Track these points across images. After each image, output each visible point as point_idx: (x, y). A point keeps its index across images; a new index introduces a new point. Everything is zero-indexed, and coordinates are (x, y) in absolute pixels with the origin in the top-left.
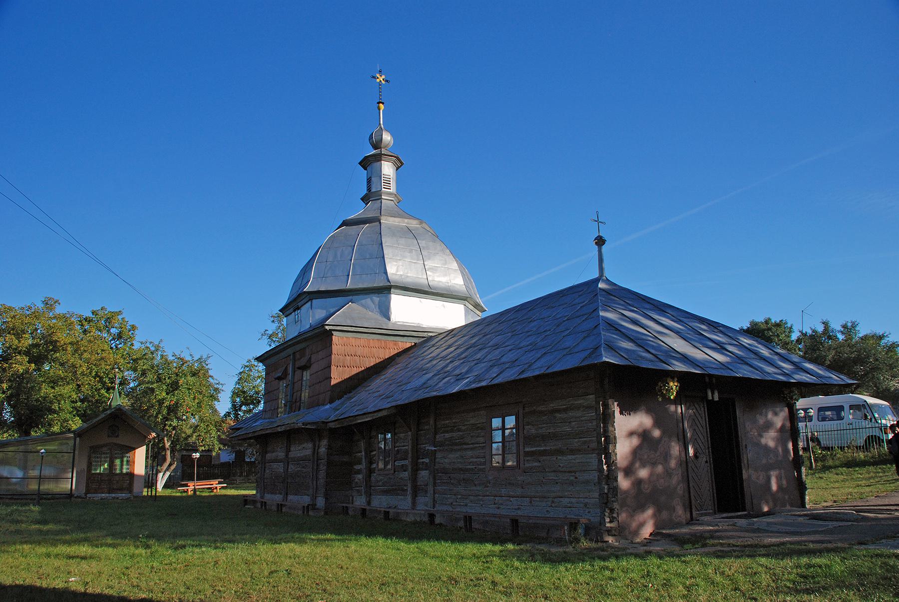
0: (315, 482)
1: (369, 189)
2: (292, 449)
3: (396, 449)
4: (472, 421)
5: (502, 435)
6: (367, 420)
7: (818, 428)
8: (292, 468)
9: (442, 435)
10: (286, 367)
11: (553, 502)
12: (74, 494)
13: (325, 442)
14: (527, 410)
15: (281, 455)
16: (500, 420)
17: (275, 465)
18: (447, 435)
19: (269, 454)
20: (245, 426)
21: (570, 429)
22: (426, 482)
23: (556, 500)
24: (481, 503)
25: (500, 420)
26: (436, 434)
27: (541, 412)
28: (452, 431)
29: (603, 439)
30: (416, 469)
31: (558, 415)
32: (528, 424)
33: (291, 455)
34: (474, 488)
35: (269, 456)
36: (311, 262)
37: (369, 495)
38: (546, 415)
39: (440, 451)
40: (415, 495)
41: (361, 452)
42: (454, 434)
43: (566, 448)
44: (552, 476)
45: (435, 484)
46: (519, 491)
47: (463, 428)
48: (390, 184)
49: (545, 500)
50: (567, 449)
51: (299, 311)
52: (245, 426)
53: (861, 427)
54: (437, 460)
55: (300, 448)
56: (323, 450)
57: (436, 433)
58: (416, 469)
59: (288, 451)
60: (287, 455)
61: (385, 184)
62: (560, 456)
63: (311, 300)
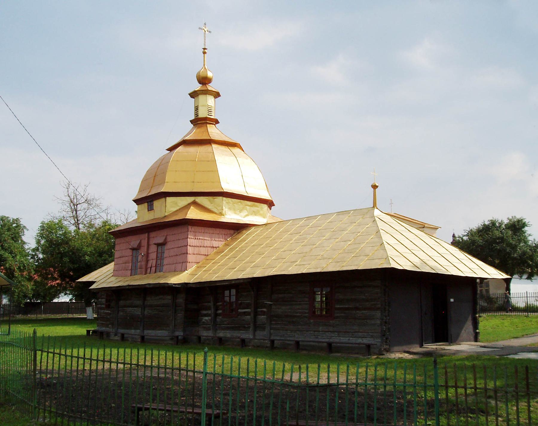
7: (520, 295)
18: (280, 296)
19: (122, 302)
24: (305, 335)
29: (39, 301)
30: (256, 314)
36: (316, 217)
40: (255, 330)
41: (209, 302)
46: (331, 329)
47: (293, 292)
48: (208, 111)
53: (522, 296)
58: (256, 314)
60: (144, 304)
61: (209, 112)
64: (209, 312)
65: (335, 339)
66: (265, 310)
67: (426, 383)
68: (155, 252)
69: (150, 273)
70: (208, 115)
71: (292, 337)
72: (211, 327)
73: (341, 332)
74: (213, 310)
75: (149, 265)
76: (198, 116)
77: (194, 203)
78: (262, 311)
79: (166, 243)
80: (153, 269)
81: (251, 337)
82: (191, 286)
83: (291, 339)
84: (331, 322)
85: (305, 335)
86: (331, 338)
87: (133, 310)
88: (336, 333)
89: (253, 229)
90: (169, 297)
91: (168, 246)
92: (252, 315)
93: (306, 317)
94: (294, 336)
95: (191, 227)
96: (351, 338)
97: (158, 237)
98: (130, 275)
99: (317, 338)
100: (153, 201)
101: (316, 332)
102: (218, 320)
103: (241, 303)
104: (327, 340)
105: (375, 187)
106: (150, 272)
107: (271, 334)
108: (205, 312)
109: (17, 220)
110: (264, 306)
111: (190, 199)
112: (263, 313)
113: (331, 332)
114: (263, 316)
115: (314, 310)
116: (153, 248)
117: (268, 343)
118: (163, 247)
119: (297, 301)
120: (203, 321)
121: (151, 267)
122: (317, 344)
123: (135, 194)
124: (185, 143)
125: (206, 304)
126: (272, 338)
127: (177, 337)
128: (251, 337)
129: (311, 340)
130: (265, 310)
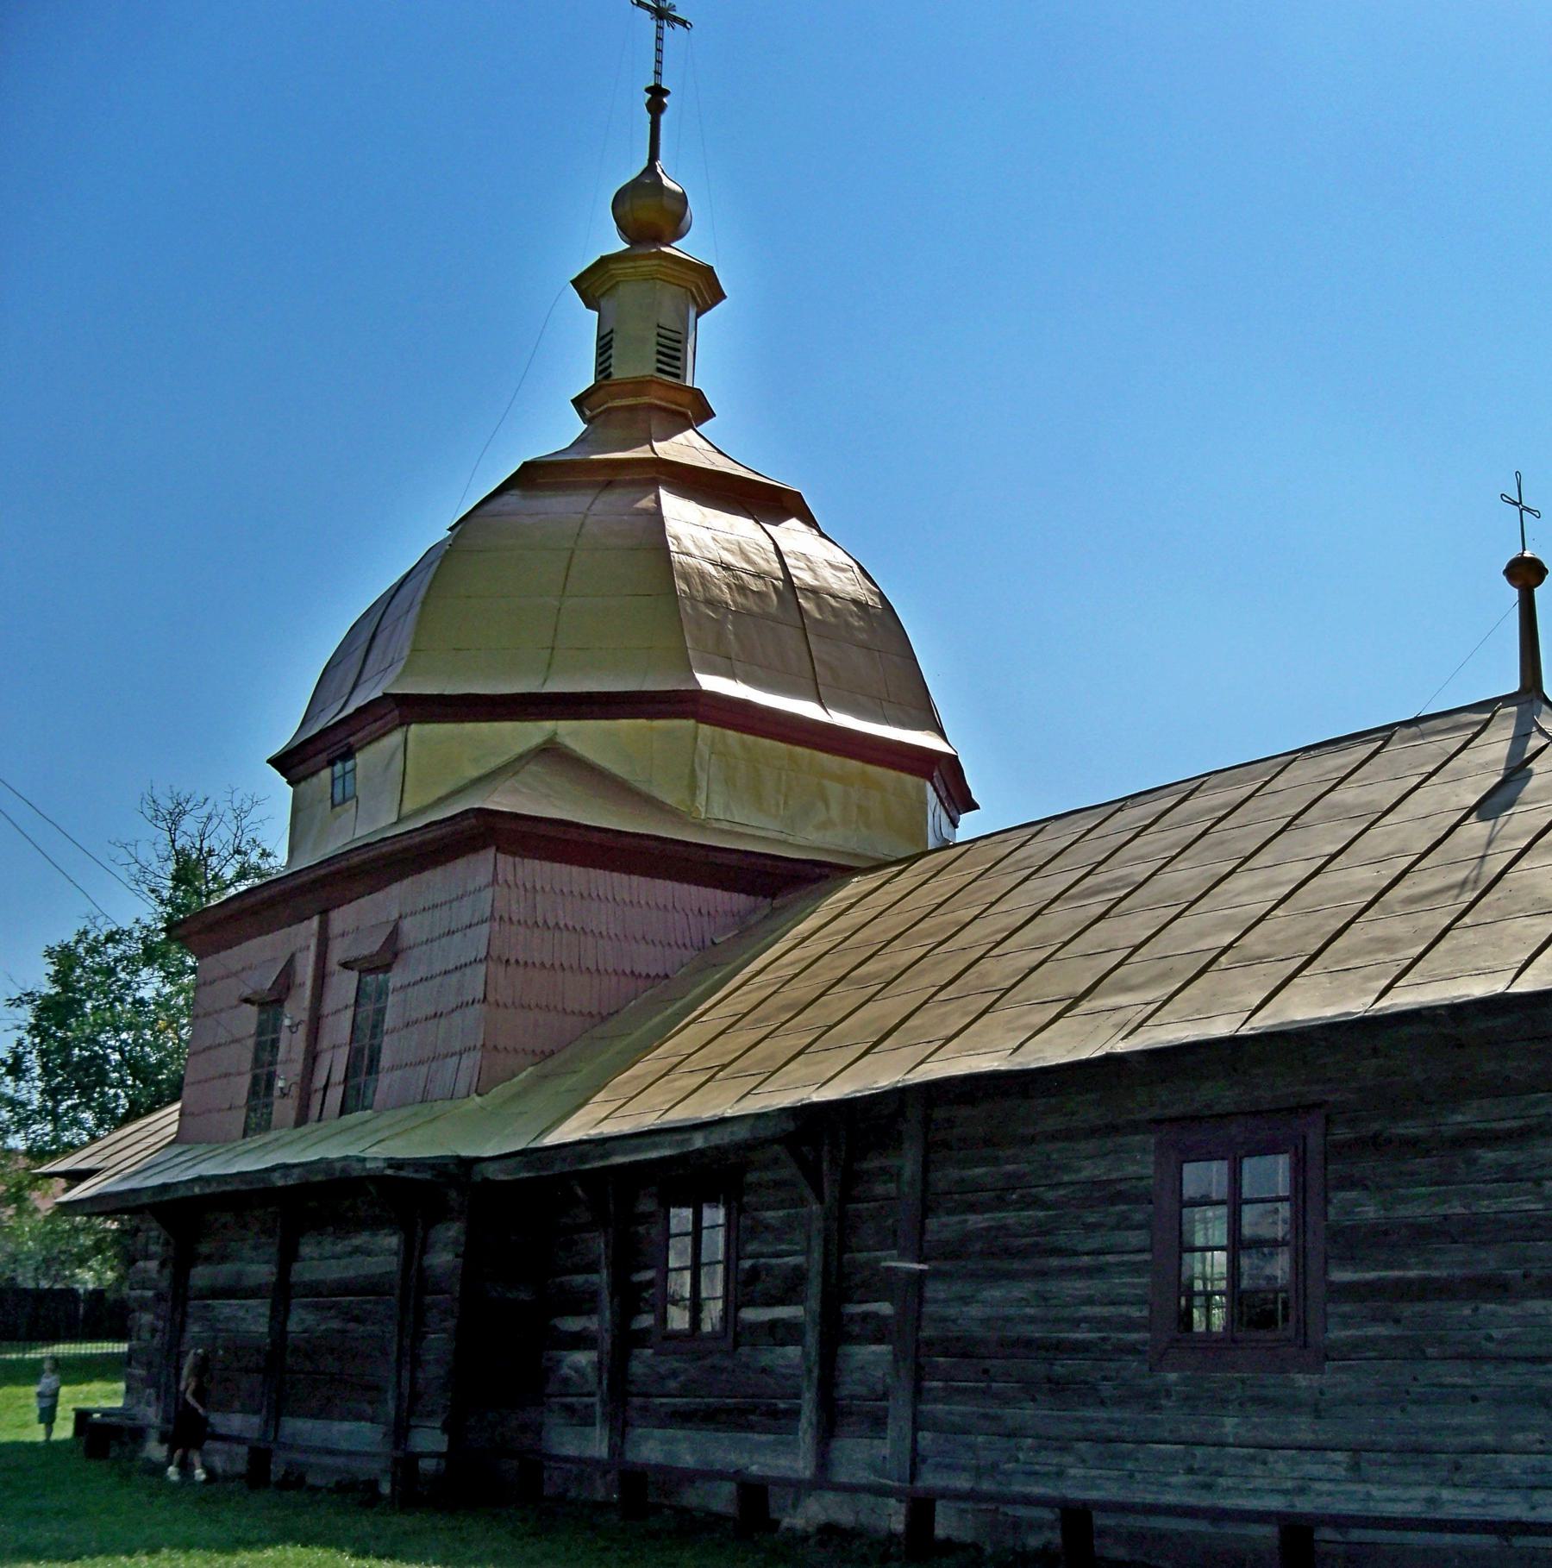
0: (406, 1374)
1: (603, 370)
2: (306, 1250)
3: (747, 1264)
4: (1090, 1171)
5: (700, 1249)
6: (654, 1155)
8: (300, 1320)
9: (955, 1219)
10: (291, 960)
11: (1457, 1467)
12: (632, 1382)
13: (452, 1231)
14: (1342, 1133)
15: (262, 1271)
16: (688, 1213)
17: (225, 1308)
18: (976, 1221)
19: (200, 1268)
20: (109, 1163)
21: (1540, 1206)
22: (880, 1388)
23: (1466, 1461)
24: (1129, 1466)
25: (688, 1213)
26: (925, 1216)
27: (1412, 1143)
28: (1000, 1203)
31: (1488, 1156)
32: (1348, 1183)
33: (303, 1272)
34: (1103, 1414)
35: (201, 1275)
37: (620, 1427)
38: (1427, 1153)
39: (937, 1274)
40: (828, 1429)
41: (592, 1268)
42: (1010, 1217)
43: (1518, 1272)
44: (1455, 1375)
45: (918, 1393)
46: (1303, 1428)
48: (659, 335)
49: (1422, 1458)
50: (1526, 1276)
51: (349, 765)
52: (109, 1163)
54: (928, 1309)
55: (339, 1248)
56: (442, 1259)
57: (927, 1210)
59: (288, 1256)
62: (1487, 1301)
63: (404, 722)
64: (591, 1323)
65: (1330, 1494)
66: (885, 1308)
67: (129, 1251)
68: (346, 1007)
69: (319, 1120)
71: (1045, 1474)
72: (598, 1408)
73: (1372, 1447)
74: (608, 1314)
75: (319, 1082)
76: (610, 375)
77: (550, 751)
78: (866, 1317)
80: (335, 1096)
83: (1037, 1490)
84: (1302, 1379)
85: (1129, 1466)
86: (1301, 1491)
87: (241, 1314)
88: (1338, 1456)
90: (393, 1241)
92: (811, 1338)
93: (1132, 1349)
94: (1060, 1474)
95: (510, 859)
98: (241, 1133)
99: (1208, 1487)
101: (1199, 1451)
102: (637, 1368)
103: (754, 1273)
104: (1275, 1503)
107: (916, 1460)
108: (572, 1324)
110: (885, 1285)
111: (534, 732)
112: (879, 1331)
113: (1300, 1448)
115: (1183, 1301)
116: (344, 985)
119: (1076, 1253)
121: (326, 1088)
122: (1202, 1526)
125: (579, 1279)
126: (930, 1479)
129: (1170, 1498)
130: (885, 1308)
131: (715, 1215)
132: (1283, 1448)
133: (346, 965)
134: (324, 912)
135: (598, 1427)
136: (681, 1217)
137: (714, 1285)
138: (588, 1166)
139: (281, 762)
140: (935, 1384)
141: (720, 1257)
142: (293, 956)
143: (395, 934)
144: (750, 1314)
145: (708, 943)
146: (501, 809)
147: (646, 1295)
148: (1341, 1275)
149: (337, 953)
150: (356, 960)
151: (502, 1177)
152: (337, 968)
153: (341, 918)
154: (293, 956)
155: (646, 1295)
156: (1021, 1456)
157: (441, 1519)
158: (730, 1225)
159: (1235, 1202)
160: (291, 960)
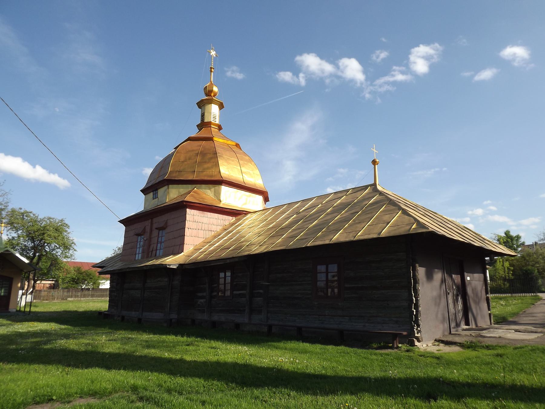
3: (235, 283)
10: (145, 228)
51: (156, 192)
64: (204, 294)
66: (261, 291)
70: (213, 120)
72: (206, 310)
75: (151, 249)
79: (167, 227)
81: (246, 321)
82: (187, 267)
89: (249, 215)
90: (166, 279)
91: (167, 230)
96: (367, 324)
97: (159, 221)
100: (157, 190)
105: (374, 162)
106: (151, 255)
108: (200, 294)
109: (62, 220)
114: (259, 298)
117: (265, 329)
118: (164, 231)
120: (199, 303)
121: (152, 251)
123: (143, 186)
124: (189, 139)
125: (202, 286)
127: (171, 320)
128: (246, 321)
130: (261, 291)
131: (228, 274)
132: (336, 316)
133: (157, 229)
134: (152, 219)
135: (206, 313)
136: (222, 275)
137: (228, 287)
138: (206, 266)
139: (143, 191)
140: (271, 305)
141: (230, 282)
142: (145, 226)
143: (166, 223)
144: (235, 292)
145: (224, 225)
146: (179, 201)
147: (215, 289)
148: (346, 286)
149: (155, 226)
150: (159, 228)
151: (189, 268)
152: (154, 229)
153: (155, 220)
154: (145, 226)
155: (215, 289)
156: (287, 318)
157: (66, 231)
158: (231, 276)
159: (327, 273)
160: (145, 228)
